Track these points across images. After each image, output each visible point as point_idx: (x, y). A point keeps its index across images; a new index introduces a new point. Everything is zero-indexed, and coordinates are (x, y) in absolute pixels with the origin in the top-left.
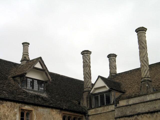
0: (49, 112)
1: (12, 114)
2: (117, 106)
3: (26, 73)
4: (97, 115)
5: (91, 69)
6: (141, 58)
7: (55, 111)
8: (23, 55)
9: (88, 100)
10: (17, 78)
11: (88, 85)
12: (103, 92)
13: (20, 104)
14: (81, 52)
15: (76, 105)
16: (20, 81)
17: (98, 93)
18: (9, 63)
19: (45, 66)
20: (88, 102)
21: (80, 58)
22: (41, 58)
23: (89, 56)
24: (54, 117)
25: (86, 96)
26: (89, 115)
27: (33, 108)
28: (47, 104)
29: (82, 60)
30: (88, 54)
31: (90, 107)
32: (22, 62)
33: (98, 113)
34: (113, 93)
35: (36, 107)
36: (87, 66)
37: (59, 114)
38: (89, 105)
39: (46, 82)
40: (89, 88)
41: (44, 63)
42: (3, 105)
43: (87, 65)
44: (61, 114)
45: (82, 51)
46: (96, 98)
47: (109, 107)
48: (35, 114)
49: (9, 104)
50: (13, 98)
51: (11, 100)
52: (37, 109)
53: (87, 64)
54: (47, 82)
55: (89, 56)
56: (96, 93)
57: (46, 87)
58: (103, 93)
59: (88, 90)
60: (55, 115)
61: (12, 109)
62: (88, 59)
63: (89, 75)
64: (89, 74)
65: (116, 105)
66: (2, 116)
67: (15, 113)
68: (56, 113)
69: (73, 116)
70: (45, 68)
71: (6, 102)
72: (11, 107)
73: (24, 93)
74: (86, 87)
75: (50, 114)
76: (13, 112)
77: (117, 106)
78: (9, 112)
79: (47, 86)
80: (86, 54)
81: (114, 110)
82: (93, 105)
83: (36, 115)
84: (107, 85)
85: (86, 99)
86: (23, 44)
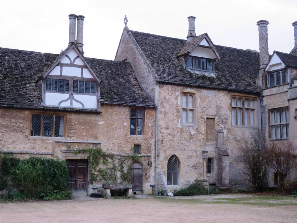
0: (215, 94)
2: (292, 87)
3: (189, 53)
4: (272, 96)
5: (268, 41)
8: (189, 31)
9: (264, 78)
10: (181, 58)
11: (264, 62)
12: (279, 69)
13: (182, 87)
15: (250, 85)
17: (273, 71)
18: (175, 40)
20: (264, 80)
21: (256, 30)
22: (206, 34)
23: (266, 27)
25: (262, 74)
26: (264, 95)
27: (196, 90)
28: (213, 86)
30: (265, 25)
31: (265, 87)
32: (188, 39)
33: (273, 93)
34: (289, 71)
35: (199, 90)
36: (263, 38)
37: (227, 96)
38: (264, 84)
39: (215, 60)
41: (210, 40)
43: (264, 38)
44: (229, 96)
45: (257, 22)
46: (272, 77)
47: (284, 87)
48: (198, 97)
49: (169, 87)
50: (173, 81)
51: (171, 83)
52: (200, 92)
53: (263, 36)
54: (215, 61)
55: (266, 27)
56: (272, 71)
57: (214, 66)
58: (279, 71)
59: (264, 67)
62: (264, 31)
63: (265, 50)
65: (291, 86)
66: (163, 99)
67: (176, 96)
68: (224, 94)
72: (171, 90)
73: (188, 74)
74: (261, 64)
76: (174, 95)
77: (292, 87)
78: (170, 96)
79: (215, 65)
80: (263, 24)
81: (287, 91)
82: (269, 84)
83: (200, 98)
84: (283, 62)
85: (262, 77)
86: (189, 18)
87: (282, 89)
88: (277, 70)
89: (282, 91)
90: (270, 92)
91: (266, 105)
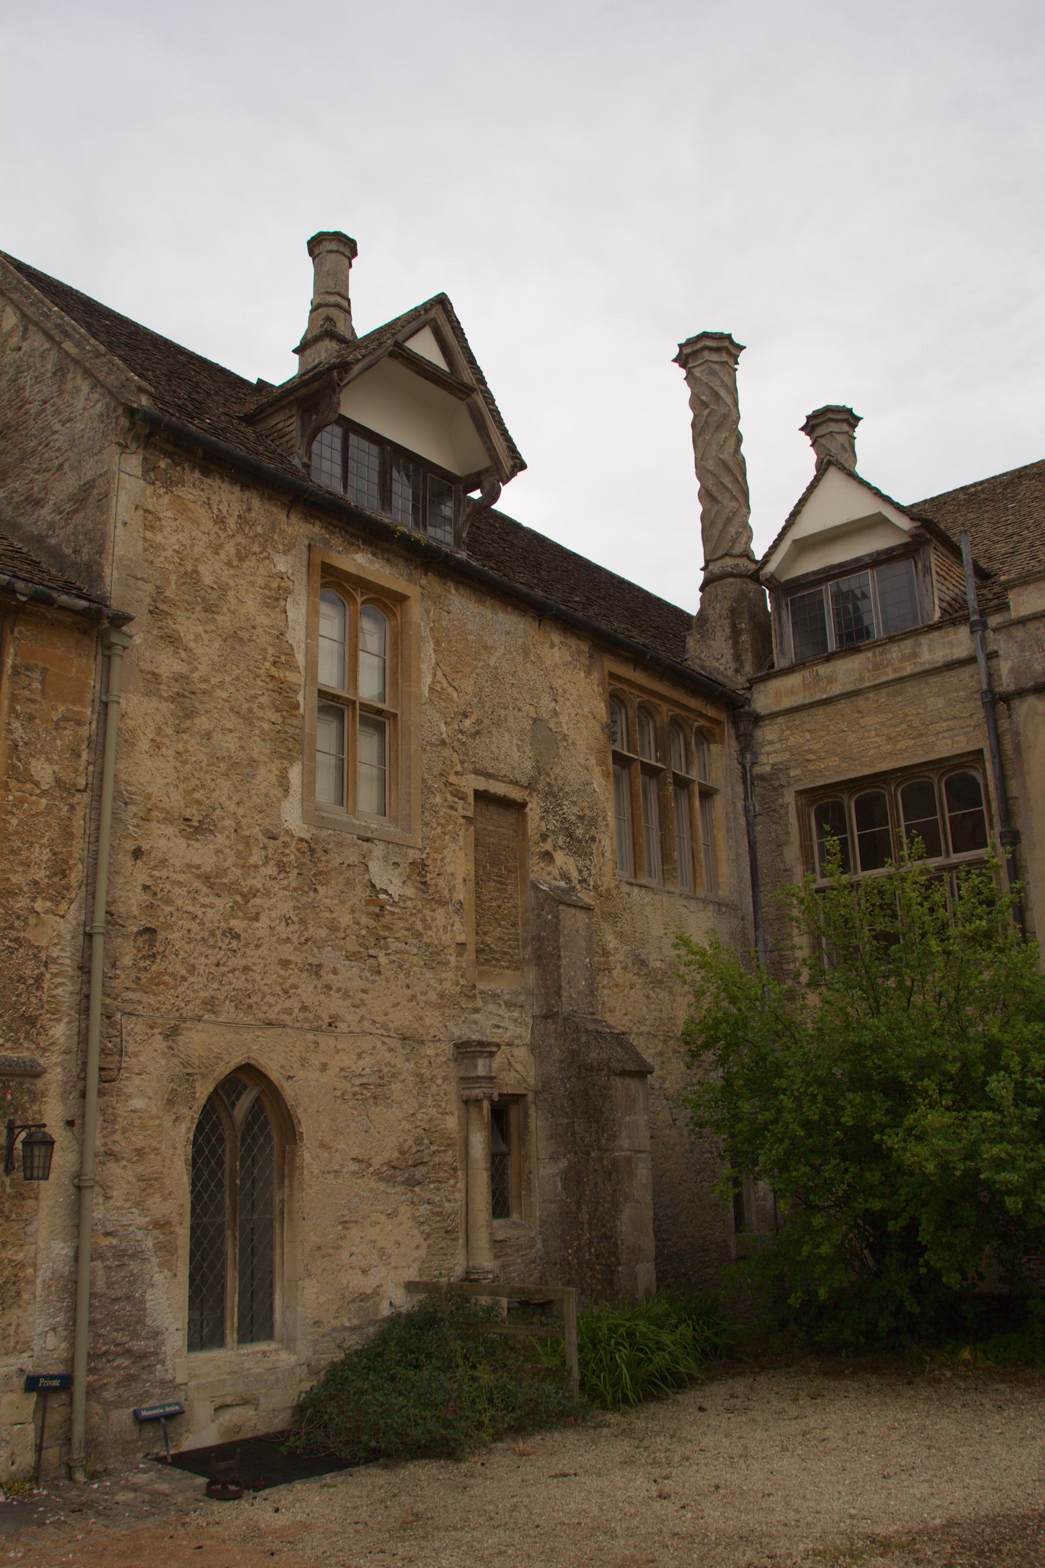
1: (252, 583)
4: (829, 709)
6: (256, 1110)
7: (561, 642)
11: (734, 541)
12: (857, 560)
14: (681, 346)
16: (303, 431)
19: (471, 360)
24: (558, 683)
27: (411, 579)
29: (686, 392)
32: (308, 352)
33: (836, 689)
35: (429, 581)
37: (588, 673)
38: (748, 658)
40: (741, 556)
42: (179, 491)
48: (426, 633)
53: (723, 411)
60: (558, 672)
61: (256, 548)
64: (736, 472)
66: (173, 578)
67: (275, 585)
69: (665, 708)
70: (467, 377)
71: (207, 476)
75: (526, 653)
78: (229, 564)
82: (782, 652)
83: (437, 643)
85: (726, 622)
87: (904, 658)
88: (840, 565)
89: (909, 669)
90: (805, 687)
91: (779, 770)
